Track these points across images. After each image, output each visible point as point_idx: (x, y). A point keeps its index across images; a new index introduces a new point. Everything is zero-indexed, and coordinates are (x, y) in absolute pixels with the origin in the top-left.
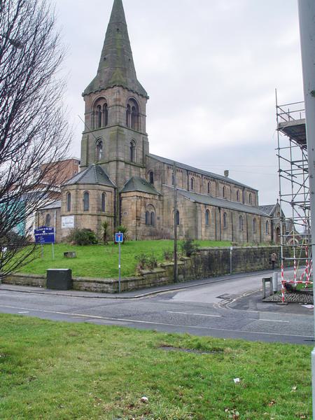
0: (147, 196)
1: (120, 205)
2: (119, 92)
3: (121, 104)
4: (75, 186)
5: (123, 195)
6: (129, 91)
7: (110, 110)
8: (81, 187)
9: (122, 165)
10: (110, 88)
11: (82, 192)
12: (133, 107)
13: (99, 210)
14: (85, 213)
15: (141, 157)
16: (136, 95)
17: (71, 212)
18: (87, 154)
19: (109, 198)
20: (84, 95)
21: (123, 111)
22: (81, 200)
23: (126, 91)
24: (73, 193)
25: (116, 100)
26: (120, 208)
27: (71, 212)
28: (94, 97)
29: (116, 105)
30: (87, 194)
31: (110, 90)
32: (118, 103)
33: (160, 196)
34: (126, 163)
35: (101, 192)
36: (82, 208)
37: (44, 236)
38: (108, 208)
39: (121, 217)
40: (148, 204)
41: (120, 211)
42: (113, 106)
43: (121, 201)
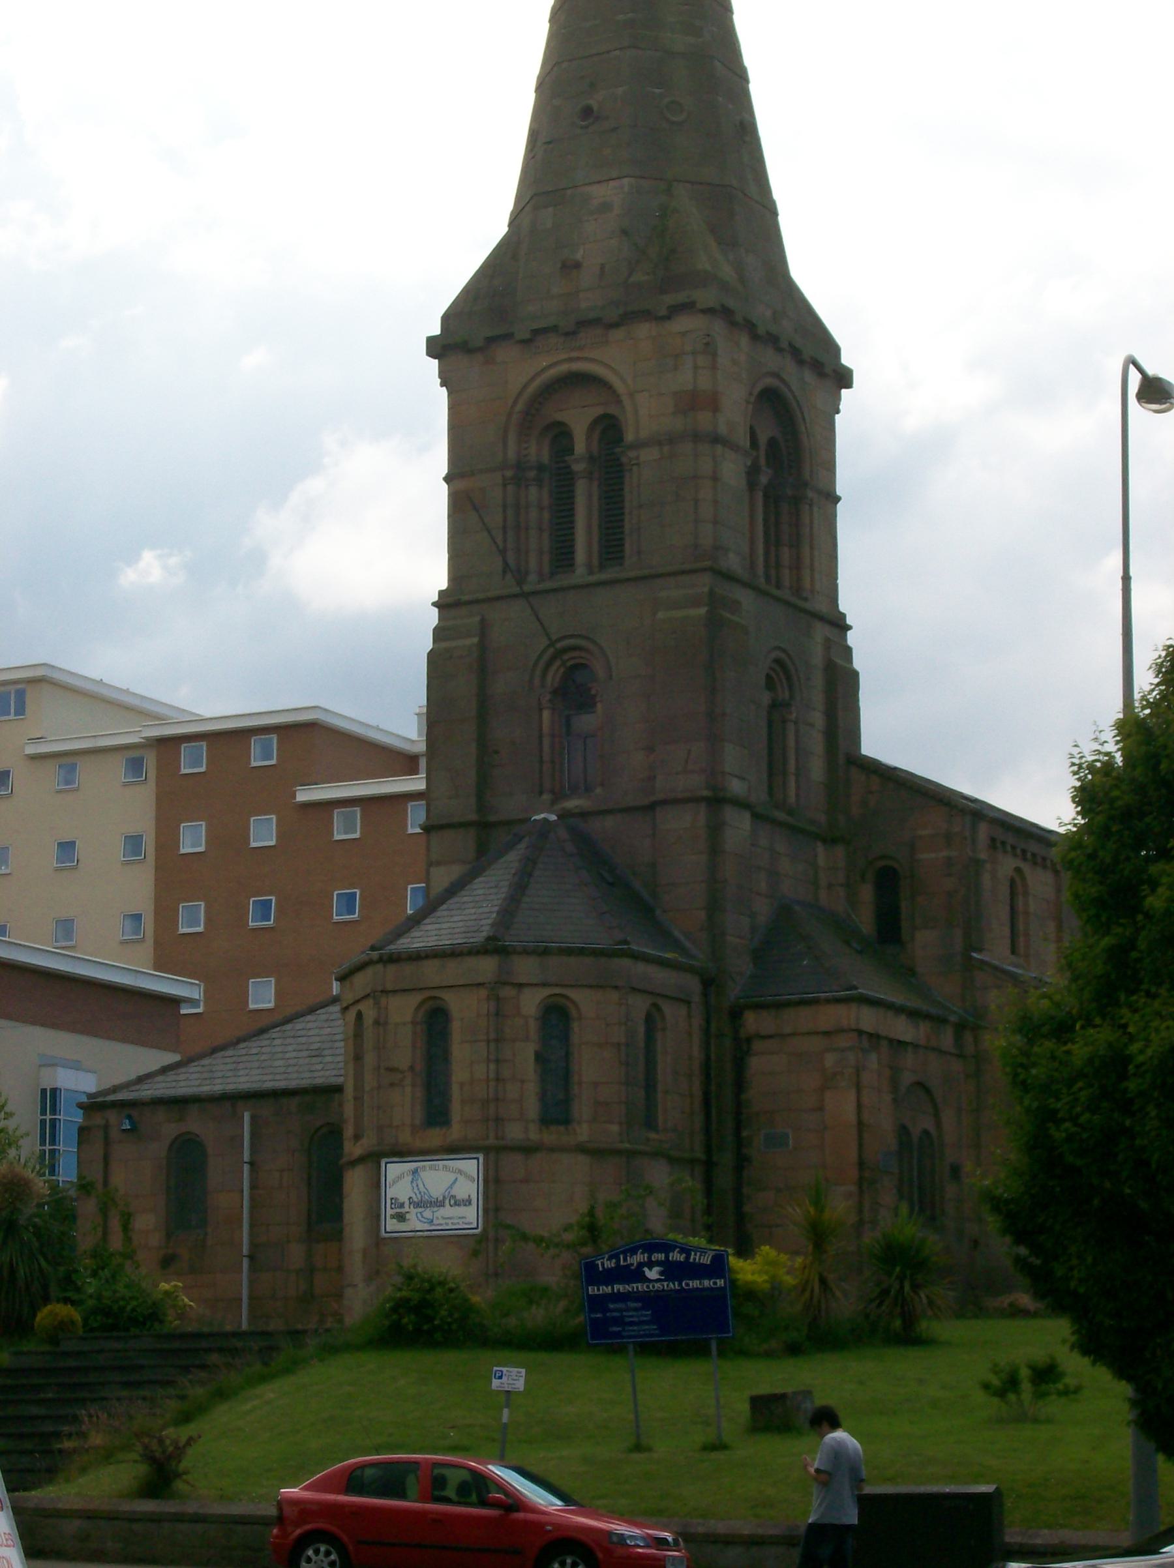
0: (902, 1029)
1: (740, 1084)
2: (709, 348)
3: (723, 429)
4: (487, 967)
5: (752, 1021)
6: (755, 337)
7: (645, 472)
8: (525, 968)
9: (739, 826)
10: (647, 315)
11: (531, 1002)
12: (772, 443)
13: (546, 1121)
14: (550, 1137)
15: (817, 769)
16: (790, 370)
17: (456, 1132)
18: (1013, 909)
19: (681, 1041)
20: (435, 347)
21: (732, 470)
22: (524, 1056)
23: (744, 340)
24: (465, 1009)
25: (694, 402)
26: (739, 1105)
27: (456, 1132)
28: (523, 371)
29: (697, 437)
30: (557, 1017)
31: (644, 330)
32: (704, 419)
33: (960, 1028)
34: (756, 816)
35: (640, 1005)
36: (532, 1108)
37: (647, 1300)
38: (677, 1106)
39: (742, 1162)
40: (907, 1078)
41: (738, 1129)
42: (671, 439)
43: (740, 1064)
